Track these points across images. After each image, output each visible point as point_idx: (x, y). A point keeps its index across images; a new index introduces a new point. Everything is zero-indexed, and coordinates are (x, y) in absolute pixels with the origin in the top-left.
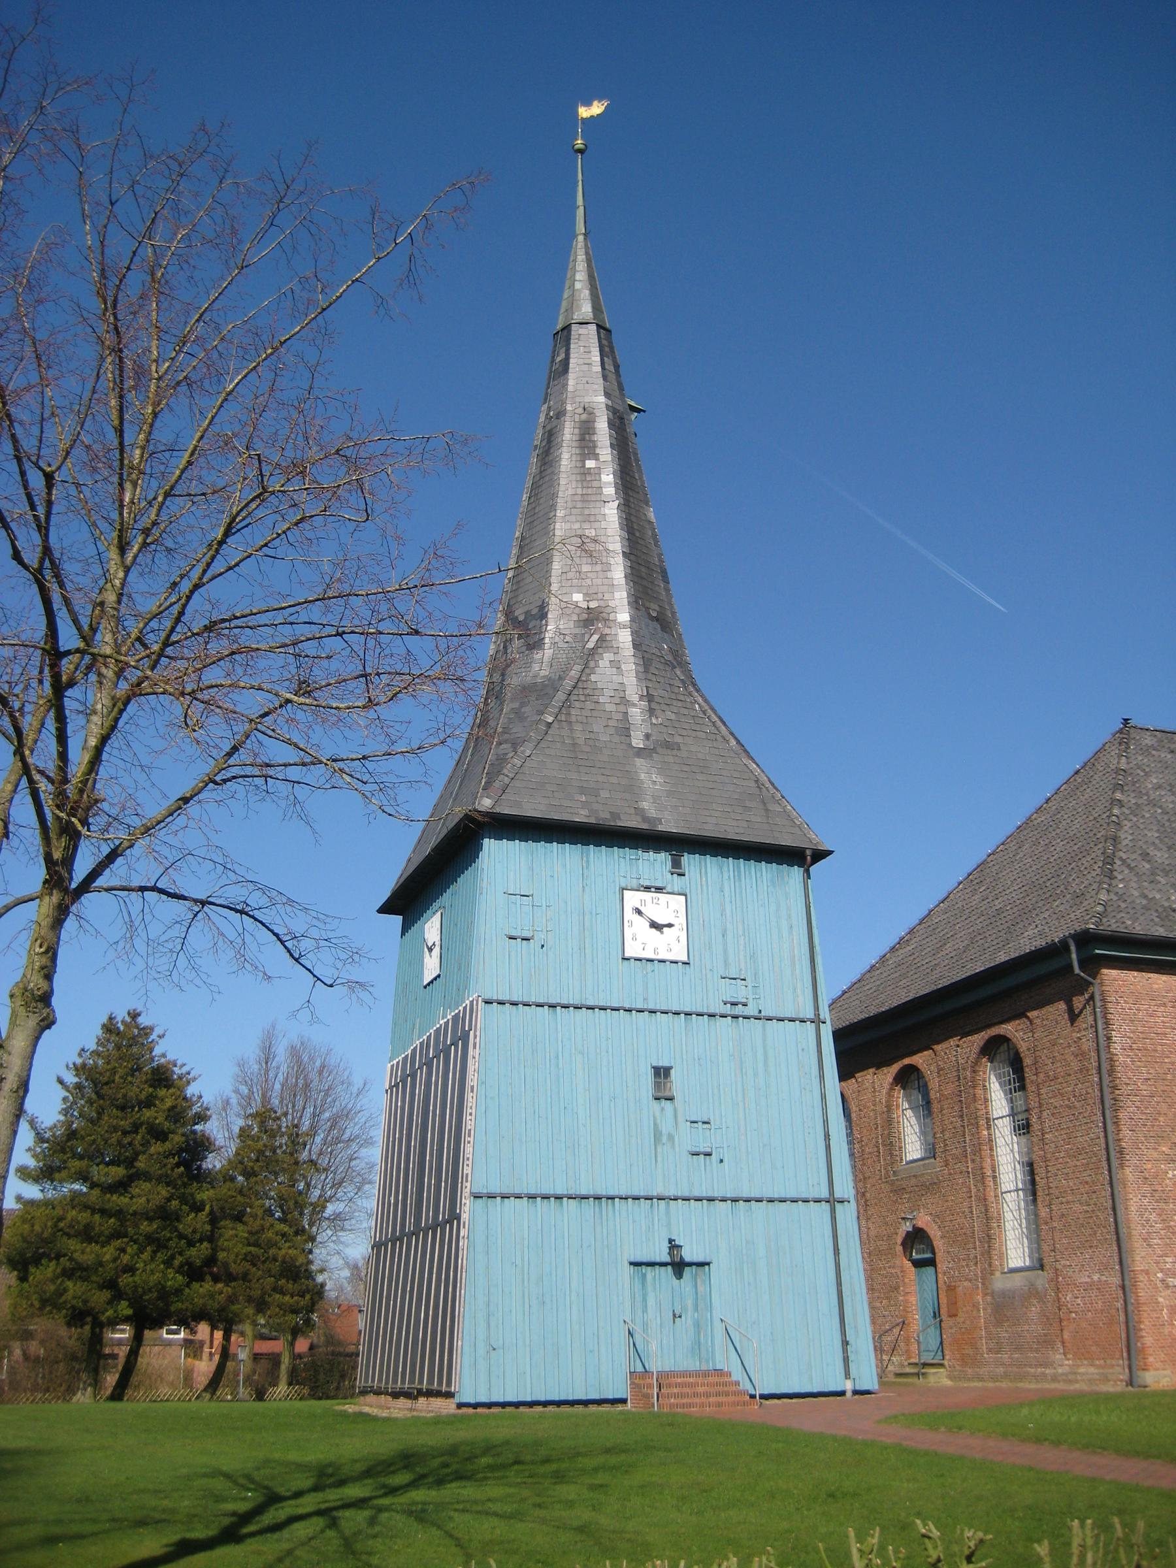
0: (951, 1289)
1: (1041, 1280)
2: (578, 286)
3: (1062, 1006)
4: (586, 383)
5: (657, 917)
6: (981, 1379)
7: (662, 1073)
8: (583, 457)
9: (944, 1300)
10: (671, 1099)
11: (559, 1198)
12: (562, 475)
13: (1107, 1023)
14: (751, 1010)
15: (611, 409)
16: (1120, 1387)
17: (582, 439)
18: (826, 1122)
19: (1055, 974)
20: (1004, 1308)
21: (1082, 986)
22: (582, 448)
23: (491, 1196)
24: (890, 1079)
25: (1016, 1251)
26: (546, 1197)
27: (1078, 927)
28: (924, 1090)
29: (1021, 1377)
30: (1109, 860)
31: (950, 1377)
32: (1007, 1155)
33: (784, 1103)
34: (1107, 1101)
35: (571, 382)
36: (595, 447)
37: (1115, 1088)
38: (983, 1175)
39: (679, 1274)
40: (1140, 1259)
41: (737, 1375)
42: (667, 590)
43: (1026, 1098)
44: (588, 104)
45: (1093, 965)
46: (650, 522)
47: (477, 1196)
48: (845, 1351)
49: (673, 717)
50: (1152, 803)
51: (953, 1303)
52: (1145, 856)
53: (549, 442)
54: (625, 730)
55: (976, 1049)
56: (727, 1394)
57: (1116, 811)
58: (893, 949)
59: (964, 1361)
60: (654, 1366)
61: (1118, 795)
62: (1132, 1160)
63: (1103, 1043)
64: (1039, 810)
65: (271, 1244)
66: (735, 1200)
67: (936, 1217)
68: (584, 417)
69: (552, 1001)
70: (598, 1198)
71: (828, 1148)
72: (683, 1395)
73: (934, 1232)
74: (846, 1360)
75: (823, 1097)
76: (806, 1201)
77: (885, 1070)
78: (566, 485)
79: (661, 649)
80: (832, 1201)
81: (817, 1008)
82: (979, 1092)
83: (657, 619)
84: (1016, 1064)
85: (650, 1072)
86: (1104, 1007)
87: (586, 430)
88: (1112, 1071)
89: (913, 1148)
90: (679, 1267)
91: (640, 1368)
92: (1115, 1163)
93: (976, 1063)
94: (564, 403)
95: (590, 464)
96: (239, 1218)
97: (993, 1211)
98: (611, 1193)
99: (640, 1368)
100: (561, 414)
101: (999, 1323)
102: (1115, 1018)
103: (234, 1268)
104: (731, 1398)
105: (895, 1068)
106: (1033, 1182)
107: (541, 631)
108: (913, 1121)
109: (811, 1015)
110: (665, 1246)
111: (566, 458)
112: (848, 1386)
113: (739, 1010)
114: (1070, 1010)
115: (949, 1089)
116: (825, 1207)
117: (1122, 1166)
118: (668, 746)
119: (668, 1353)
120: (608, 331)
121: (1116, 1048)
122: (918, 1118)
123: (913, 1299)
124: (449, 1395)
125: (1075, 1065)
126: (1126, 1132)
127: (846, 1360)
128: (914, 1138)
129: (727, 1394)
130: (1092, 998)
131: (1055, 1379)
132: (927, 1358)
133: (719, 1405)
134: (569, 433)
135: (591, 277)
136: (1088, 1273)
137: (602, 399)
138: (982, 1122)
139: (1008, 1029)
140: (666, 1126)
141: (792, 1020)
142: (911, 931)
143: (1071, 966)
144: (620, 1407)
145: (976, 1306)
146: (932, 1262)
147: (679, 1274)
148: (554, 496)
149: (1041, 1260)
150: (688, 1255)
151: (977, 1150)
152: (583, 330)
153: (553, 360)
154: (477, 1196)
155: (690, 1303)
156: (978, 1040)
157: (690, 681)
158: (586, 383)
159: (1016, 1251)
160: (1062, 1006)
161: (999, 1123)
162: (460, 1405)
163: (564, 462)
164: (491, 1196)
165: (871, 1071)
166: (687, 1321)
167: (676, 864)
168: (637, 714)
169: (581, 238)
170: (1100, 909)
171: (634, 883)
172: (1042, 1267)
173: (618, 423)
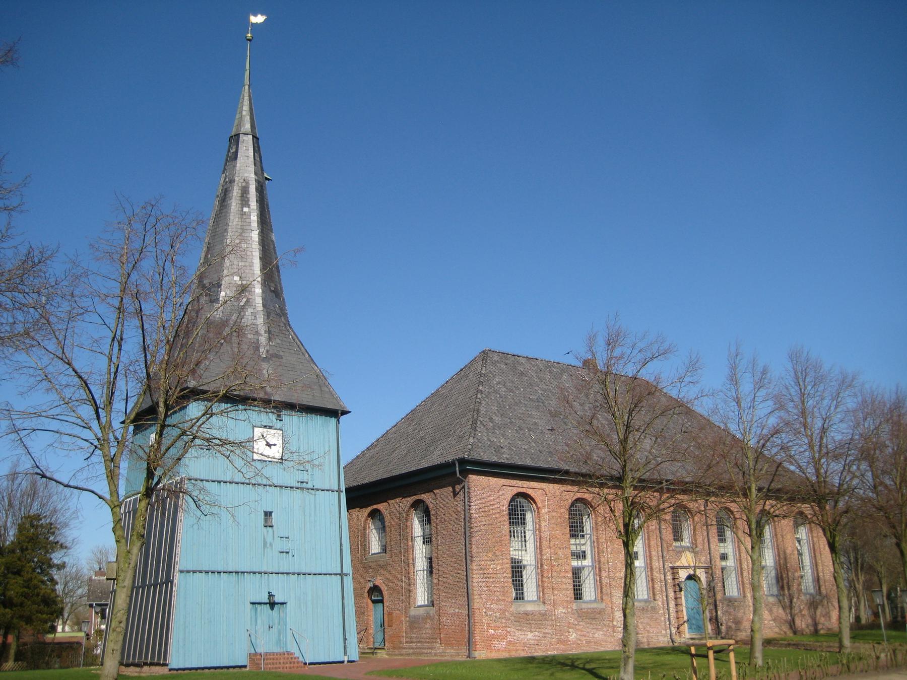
0: (390, 614)
1: (432, 611)
2: (244, 113)
3: (450, 489)
4: (245, 167)
5: (269, 439)
6: (402, 655)
7: (268, 514)
8: (243, 206)
9: (386, 619)
10: (272, 527)
11: (219, 572)
12: (232, 214)
13: (469, 499)
14: (310, 486)
15: (257, 181)
16: (464, 659)
17: (242, 196)
18: (341, 538)
19: (450, 474)
20: (414, 623)
21: (460, 482)
22: (242, 201)
23: (188, 572)
24: (366, 514)
25: (421, 597)
26: (213, 572)
27: (460, 456)
28: (382, 520)
29: (420, 654)
30: (475, 422)
31: (387, 654)
32: (420, 553)
33: (321, 528)
34: (467, 535)
35: (238, 165)
36: (248, 201)
37: (471, 528)
38: (408, 564)
39: (272, 608)
40: (477, 603)
41: (297, 654)
42: (279, 276)
43: (431, 530)
44: (255, 15)
45: (465, 473)
46: (273, 241)
47: (181, 572)
48: (345, 643)
49: (279, 342)
50: (496, 392)
51: (390, 621)
52: (491, 419)
53: (225, 195)
54: (257, 348)
55: (409, 505)
56: (294, 663)
57: (479, 396)
58: (368, 449)
59: (394, 647)
60: (259, 650)
61: (480, 388)
62: (476, 560)
63: (467, 508)
64: (442, 386)
65: (36, 587)
66: (299, 574)
67: (384, 581)
68: (244, 184)
69: (219, 479)
70: (237, 573)
71: (341, 550)
72: (274, 664)
73: (383, 588)
74: (345, 647)
75: (340, 527)
76: (330, 575)
77: (364, 510)
78: (234, 220)
79: (275, 307)
80: (342, 575)
81: (339, 485)
82: (409, 524)
83: (274, 291)
84: (427, 512)
85: (263, 514)
86: (469, 492)
87: (245, 191)
88: (470, 521)
89: (375, 547)
90: (272, 605)
91: (253, 651)
92: (468, 561)
93: (409, 511)
94: (234, 175)
95: (246, 209)
96: (18, 573)
97: (412, 579)
98: (243, 570)
99: (253, 651)
100: (232, 181)
101: (412, 630)
102: (473, 497)
103: (15, 600)
104: (296, 665)
105: (369, 509)
106: (431, 567)
107: (218, 294)
108: (376, 535)
109: (336, 488)
110: (267, 596)
111: (234, 204)
112: (346, 659)
113: (304, 485)
114: (454, 491)
115: (395, 522)
116: (339, 577)
117: (472, 562)
118: (277, 356)
119: (266, 645)
120: (258, 139)
121: (473, 511)
122: (379, 534)
123: (371, 618)
124: (165, 665)
125: (454, 517)
126: (474, 548)
127: (345, 647)
128: (376, 543)
129: (294, 663)
130: (464, 487)
131: (435, 655)
132: (377, 645)
133: (291, 667)
134: (236, 192)
135: (251, 109)
136: (453, 609)
137: (253, 176)
138: (410, 538)
139: (425, 497)
140: (269, 539)
141: (328, 491)
142: (377, 440)
143: (455, 472)
144: (244, 669)
145: (401, 622)
146: (382, 601)
147: (272, 608)
148: (227, 224)
149: (433, 602)
150: (277, 600)
151: (406, 551)
152: (245, 138)
153: (229, 151)
154: (181, 572)
155: (276, 621)
156: (410, 500)
157: (287, 324)
158: (245, 167)
159: (421, 597)
160: (450, 489)
161: (417, 539)
162: (170, 670)
163: (233, 207)
164: (188, 572)
165: (357, 509)
166: (275, 630)
167: (279, 416)
168: (263, 339)
169: (247, 87)
170: (470, 447)
171: (259, 424)
172: (433, 605)
173: (260, 189)
